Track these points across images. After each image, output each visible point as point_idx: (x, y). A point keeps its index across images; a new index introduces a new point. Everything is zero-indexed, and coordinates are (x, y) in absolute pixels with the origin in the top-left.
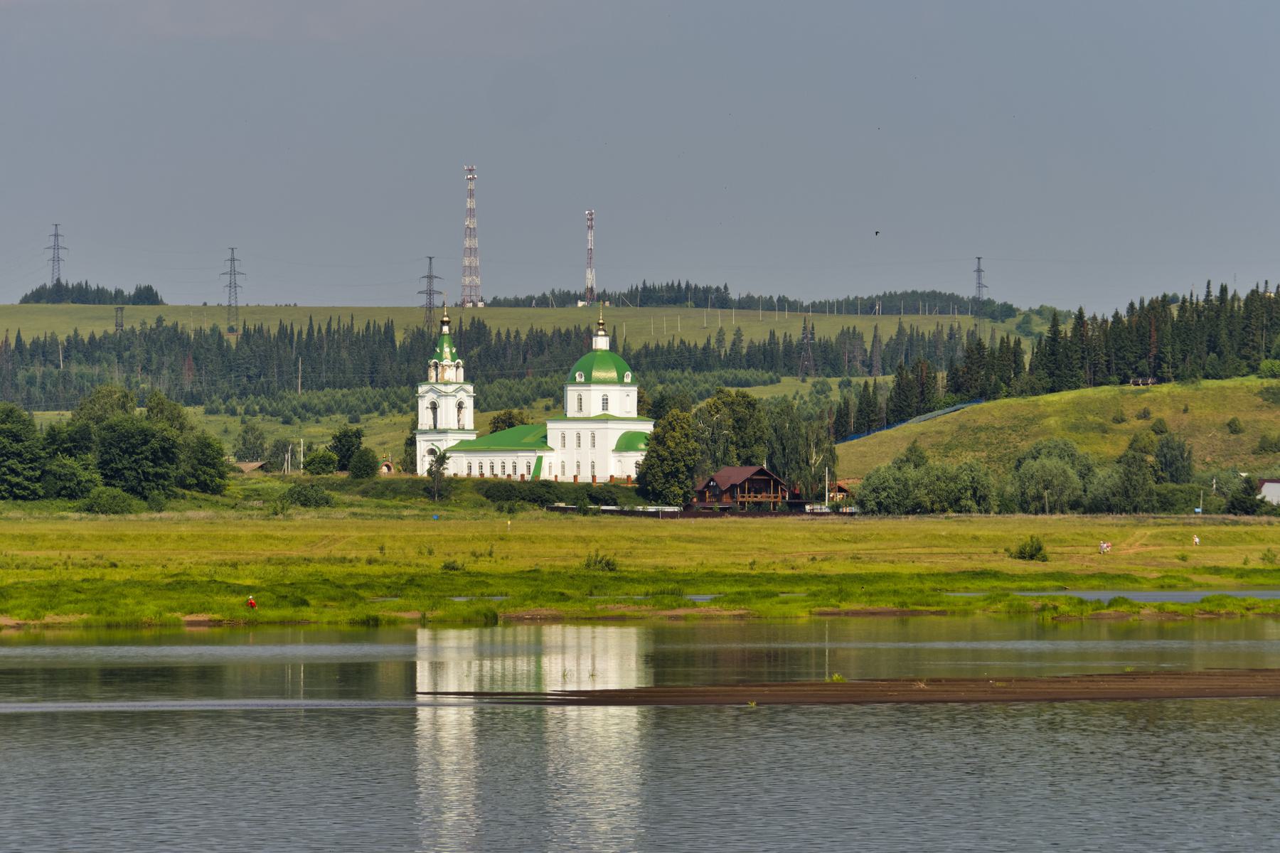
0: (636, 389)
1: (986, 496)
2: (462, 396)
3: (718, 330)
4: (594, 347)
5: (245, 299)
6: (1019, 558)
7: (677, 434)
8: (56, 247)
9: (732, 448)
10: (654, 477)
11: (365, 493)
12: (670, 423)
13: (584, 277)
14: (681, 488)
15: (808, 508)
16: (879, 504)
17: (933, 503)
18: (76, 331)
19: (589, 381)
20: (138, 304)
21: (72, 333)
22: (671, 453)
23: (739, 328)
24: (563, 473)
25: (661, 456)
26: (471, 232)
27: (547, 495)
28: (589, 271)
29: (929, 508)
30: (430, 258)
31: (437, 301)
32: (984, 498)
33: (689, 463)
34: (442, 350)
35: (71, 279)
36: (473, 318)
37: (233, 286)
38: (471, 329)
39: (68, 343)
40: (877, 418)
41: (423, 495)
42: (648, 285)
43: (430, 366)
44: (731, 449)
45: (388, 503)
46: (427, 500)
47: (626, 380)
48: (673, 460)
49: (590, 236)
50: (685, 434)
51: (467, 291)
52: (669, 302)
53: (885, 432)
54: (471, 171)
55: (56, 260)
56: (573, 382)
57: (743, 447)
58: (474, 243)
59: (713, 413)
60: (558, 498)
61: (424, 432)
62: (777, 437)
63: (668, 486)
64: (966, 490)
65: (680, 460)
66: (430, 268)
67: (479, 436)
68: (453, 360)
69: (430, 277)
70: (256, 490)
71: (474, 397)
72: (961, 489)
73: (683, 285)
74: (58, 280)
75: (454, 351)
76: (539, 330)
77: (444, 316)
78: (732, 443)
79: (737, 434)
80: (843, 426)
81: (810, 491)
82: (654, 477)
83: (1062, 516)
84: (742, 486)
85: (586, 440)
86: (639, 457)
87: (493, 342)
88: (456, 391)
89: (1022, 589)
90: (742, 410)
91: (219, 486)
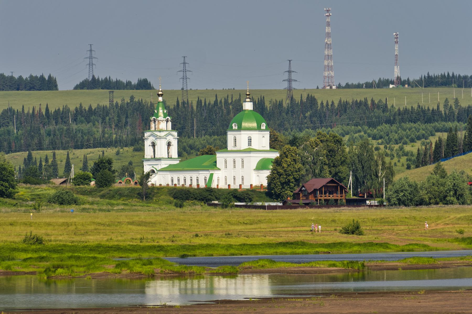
0: (269, 133)
1: (463, 194)
2: (170, 138)
3: (445, 100)
4: (244, 109)
5: (192, 85)
6: (345, 233)
7: (289, 160)
8: (91, 58)
9: (326, 167)
10: (275, 185)
11: (103, 197)
12: (285, 153)
13: (393, 71)
14: (292, 192)
15: (368, 202)
16: (399, 200)
17: (430, 199)
18: (81, 105)
19: (240, 129)
20: (139, 89)
21: (78, 106)
22: (285, 171)
23: (447, 98)
24: (234, 183)
25: (279, 172)
26: (328, 46)
27: (210, 197)
28: (396, 67)
29: (428, 202)
30: (184, 57)
31: (294, 85)
32: (461, 195)
33: (296, 176)
34: (158, 112)
35: (101, 75)
36: (308, 95)
37: (185, 78)
38: (307, 101)
39: (76, 112)
40: (457, 149)
41: (137, 197)
42: (430, 75)
43: (151, 121)
44: (325, 168)
45: (115, 202)
46: (138, 200)
47: (262, 128)
48: (286, 175)
49: (396, 47)
50: (294, 160)
51: (327, 80)
52: (442, 85)
53: (463, 157)
54: (328, 11)
55: (91, 65)
56: (232, 130)
57: (333, 166)
58: (331, 52)
59: (314, 147)
60: (216, 198)
61: (148, 160)
62: (359, 160)
63: (283, 190)
64: (450, 191)
65: (290, 175)
66: (290, 66)
67: (180, 161)
68: (165, 117)
69: (290, 72)
70: (38, 195)
71: (178, 139)
72: (447, 190)
73: (451, 75)
74: (93, 76)
75: (165, 112)
76: (345, 101)
77: (159, 91)
78: (325, 164)
79: (329, 160)
80: (438, 154)
81: (377, 193)
82: (275, 185)
83: (459, 206)
84: (320, 190)
85: (239, 163)
86: (267, 173)
87: (319, 108)
88: (167, 135)
89: (317, 253)
90: (332, 145)
91: (11, 193)
